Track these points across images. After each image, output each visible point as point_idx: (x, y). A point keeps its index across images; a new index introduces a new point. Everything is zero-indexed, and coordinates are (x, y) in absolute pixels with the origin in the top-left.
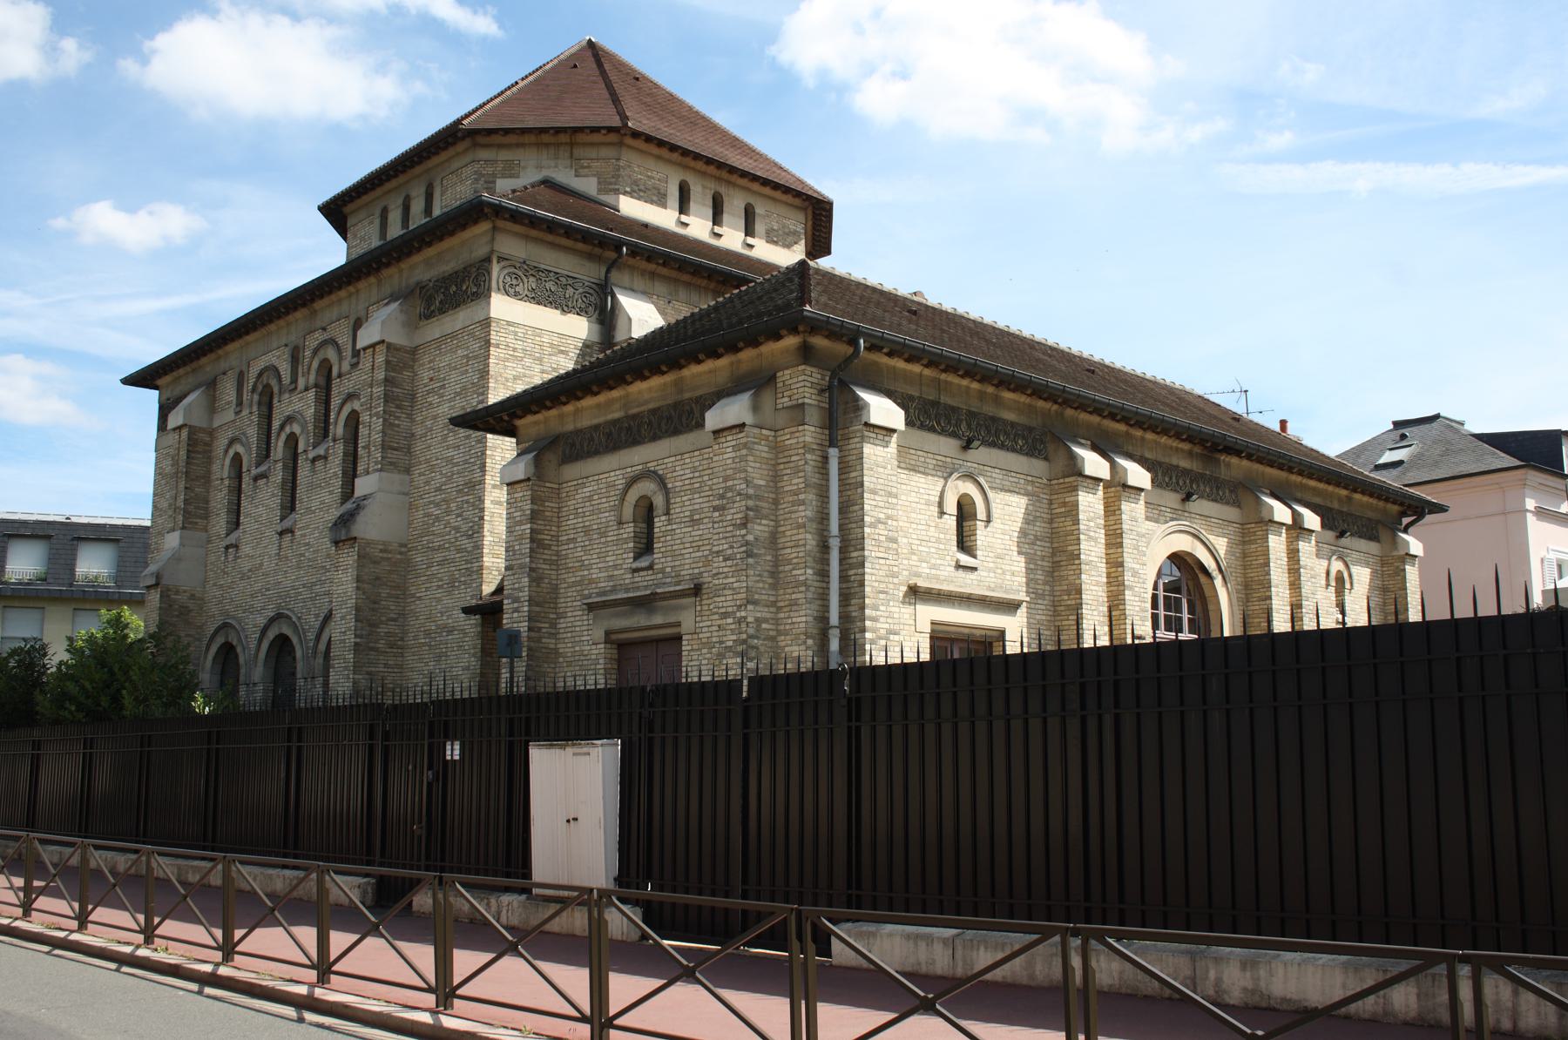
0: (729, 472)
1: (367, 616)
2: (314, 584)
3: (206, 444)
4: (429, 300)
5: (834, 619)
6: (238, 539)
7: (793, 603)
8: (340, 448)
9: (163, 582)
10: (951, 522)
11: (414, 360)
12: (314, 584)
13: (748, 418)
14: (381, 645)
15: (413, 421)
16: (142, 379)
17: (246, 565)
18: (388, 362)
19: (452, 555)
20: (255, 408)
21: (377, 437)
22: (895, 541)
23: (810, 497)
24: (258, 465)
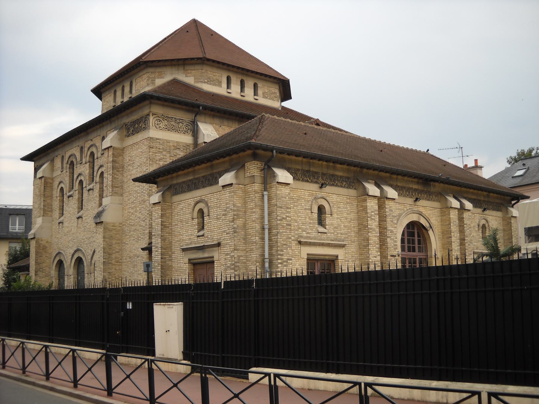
0: (228, 201)
1: (108, 252)
2: (90, 238)
3: (51, 184)
4: (128, 129)
5: (267, 256)
6: (63, 220)
7: (252, 250)
8: (98, 186)
9: (36, 237)
10: (315, 216)
11: (123, 153)
12: (90, 238)
13: (234, 181)
14: (113, 262)
15: (123, 176)
16: (28, 158)
17: (66, 230)
18: (113, 154)
19: (138, 227)
20: (68, 170)
21: (110, 183)
22: (290, 225)
23: (258, 210)
24: (69, 192)
